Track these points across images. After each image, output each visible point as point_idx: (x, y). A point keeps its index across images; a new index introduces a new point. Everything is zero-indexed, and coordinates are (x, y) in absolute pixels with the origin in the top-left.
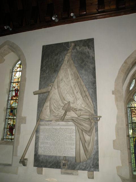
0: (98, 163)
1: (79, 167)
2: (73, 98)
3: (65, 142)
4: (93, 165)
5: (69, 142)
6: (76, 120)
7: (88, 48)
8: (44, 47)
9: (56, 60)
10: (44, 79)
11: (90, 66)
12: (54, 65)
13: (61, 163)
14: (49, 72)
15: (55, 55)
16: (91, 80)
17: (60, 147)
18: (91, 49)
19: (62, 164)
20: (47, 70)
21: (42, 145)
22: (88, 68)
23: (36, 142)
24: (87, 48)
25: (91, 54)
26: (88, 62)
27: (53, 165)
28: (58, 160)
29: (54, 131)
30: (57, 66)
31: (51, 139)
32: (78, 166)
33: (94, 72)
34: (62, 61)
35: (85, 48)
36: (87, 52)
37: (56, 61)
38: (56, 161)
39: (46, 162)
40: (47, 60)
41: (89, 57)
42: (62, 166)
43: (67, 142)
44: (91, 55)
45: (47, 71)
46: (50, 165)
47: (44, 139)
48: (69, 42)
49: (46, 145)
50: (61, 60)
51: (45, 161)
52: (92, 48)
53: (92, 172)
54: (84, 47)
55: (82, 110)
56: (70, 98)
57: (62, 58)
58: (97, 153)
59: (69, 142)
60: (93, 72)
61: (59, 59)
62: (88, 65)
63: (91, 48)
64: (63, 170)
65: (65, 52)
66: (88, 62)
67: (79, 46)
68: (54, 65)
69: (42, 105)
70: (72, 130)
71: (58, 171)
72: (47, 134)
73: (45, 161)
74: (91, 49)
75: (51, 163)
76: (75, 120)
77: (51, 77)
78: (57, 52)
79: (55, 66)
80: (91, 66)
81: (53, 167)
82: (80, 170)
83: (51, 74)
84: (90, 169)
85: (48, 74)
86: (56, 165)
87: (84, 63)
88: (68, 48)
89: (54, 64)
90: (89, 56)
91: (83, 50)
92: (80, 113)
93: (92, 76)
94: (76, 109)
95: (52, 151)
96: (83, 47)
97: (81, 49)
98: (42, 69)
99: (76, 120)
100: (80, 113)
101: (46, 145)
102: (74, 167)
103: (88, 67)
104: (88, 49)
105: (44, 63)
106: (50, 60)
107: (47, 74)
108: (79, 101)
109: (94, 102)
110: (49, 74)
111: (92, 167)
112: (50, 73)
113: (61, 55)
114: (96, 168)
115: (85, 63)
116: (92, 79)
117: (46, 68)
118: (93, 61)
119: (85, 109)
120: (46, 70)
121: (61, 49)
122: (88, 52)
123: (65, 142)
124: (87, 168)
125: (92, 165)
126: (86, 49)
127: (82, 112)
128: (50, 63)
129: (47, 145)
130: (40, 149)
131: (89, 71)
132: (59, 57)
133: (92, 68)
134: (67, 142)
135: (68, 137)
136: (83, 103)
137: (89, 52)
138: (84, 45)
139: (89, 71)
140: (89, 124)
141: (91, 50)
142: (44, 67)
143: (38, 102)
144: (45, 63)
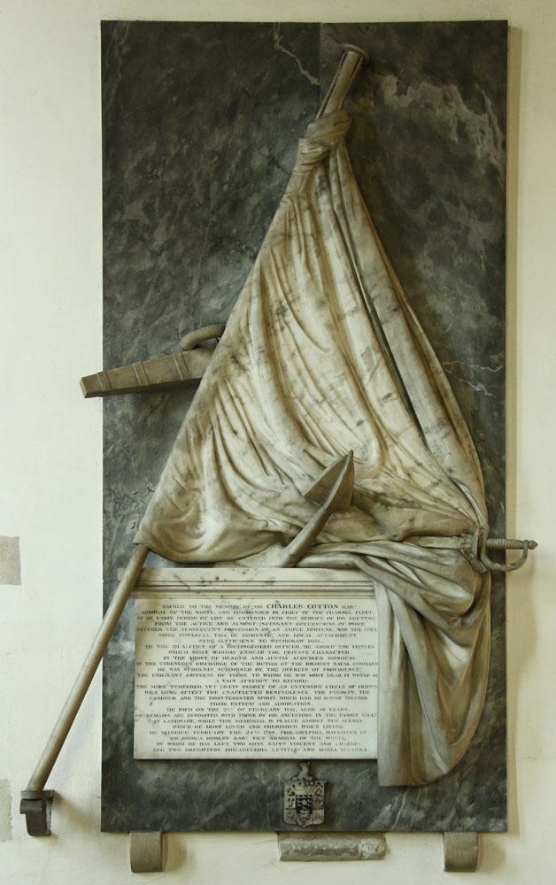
0: (500, 789)
1: (390, 814)
2: (358, 430)
3: (313, 681)
4: (472, 800)
5: (334, 681)
6: (385, 560)
7: (466, 97)
8: (115, 35)
9: (223, 157)
10: (140, 295)
11: (468, 229)
12: (207, 198)
13: (287, 797)
14: (170, 244)
15: (216, 122)
16: (474, 326)
17: (282, 711)
18: (483, 109)
19: (288, 803)
20: (157, 226)
21: (160, 707)
22: (453, 243)
23: (109, 691)
24: (458, 96)
25: (482, 148)
26: (457, 203)
27: (228, 811)
28: (264, 782)
29: (236, 620)
30: (235, 206)
31: (216, 668)
32: (388, 808)
33: (498, 273)
34: (269, 173)
35: (437, 91)
36: (455, 127)
37: (220, 169)
38: (250, 789)
39: (185, 798)
40: (151, 148)
41: (463, 165)
42: (288, 815)
43: (324, 681)
44: (479, 155)
45: (159, 240)
46: (212, 815)
47: (167, 668)
48: (319, 24)
49: (186, 704)
50: (258, 161)
51: (178, 795)
52: (489, 102)
53: (471, 836)
54: (434, 88)
55: (420, 503)
56: (341, 427)
57: (265, 151)
58: (496, 741)
59: (334, 681)
60: (490, 271)
61: (248, 154)
62: (458, 226)
63: (483, 101)
64: (295, 843)
65: (294, 108)
66: (457, 203)
67: (394, 71)
68: (213, 203)
69: (134, 465)
70: (354, 615)
71: (266, 846)
72: (188, 641)
73: (178, 795)
74: (483, 109)
75: (222, 801)
76: (374, 560)
77: (195, 285)
78: (226, 99)
79: (219, 205)
80: (479, 232)
81: (231, 821)
82: (395, 831)
83: (192, 263)
84: (456, 822)
85: (169, 259)
86: (253, 809)
87: (430, 205)
88: (315, 73)
89: (207, 185)
90: (470, 160)
91: (428, 106)
92: (412, 520)
93: (484, 304)
94: (384, 494)
95: (227, 734)
96: (425, 85)
97: (407, 100)
98: (117, 217)
99: (385, 560)
100: (412, 520)
101: (186, 704)
102: (361, 816)
103: (456, 238)
104: (464, 108)
105: (129, 166)
106: (173, 152)
107: (155, 255)
108: (396, 448)
109: (485, 461)
110: (179, 262)
111: (470, 809)
112: (179, 250)
113: (259, 124)
114: (491, 815)
115: (440, 206)
116: (478, 318)
117: (148, 208)
118: (491, 199)
119: (437, 499)
120: (151, 229)
121: (258, 81)
122: (461, 127)
123: (313, 681)
124: (442, 817)
125: (465, 799)
126: (446, 100)
127: (422, 513)
128: (174, 175)
129: (193, 704)
130: (150, 727)
131: (459, 261)
132: (246, 136)
133: (479, 246)
134: (324, 681)
135: (326, 656)
136: (420, 465)
137: (469, 128)
138: (435, 73)
139: (459, 261)
140: (345, 796)
141: (484, 117)
142: (131, 202)
143: (106, 443)
144: (139, 169)
